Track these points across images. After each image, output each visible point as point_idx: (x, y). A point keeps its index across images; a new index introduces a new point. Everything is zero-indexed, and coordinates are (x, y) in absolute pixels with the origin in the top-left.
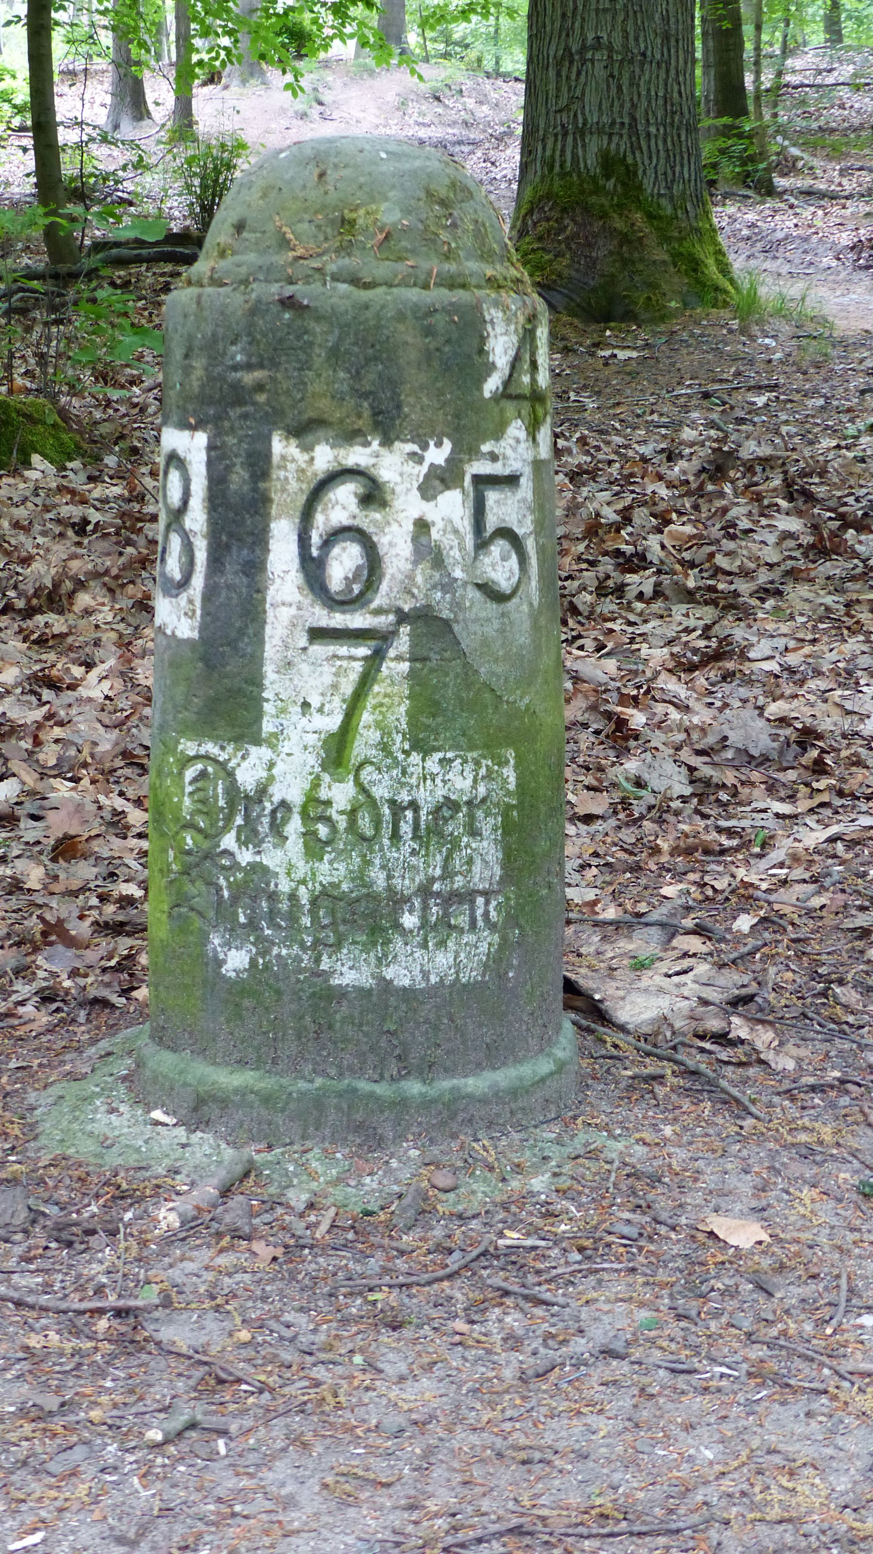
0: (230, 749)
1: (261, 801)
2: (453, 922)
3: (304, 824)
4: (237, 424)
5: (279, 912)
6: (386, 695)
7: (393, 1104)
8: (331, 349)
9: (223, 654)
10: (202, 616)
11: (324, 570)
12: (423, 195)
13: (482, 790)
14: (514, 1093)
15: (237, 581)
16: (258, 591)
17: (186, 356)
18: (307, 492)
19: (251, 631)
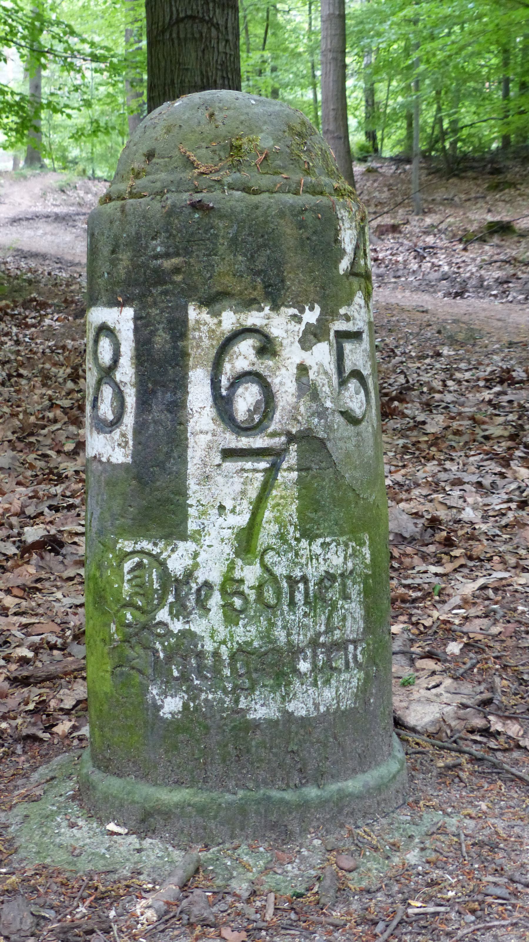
0: (161, 545)
1: (188, 583)
2: (334, 665)
3: (223, 598)
4: (158, 299)
5: (205, 666)
6: (282, 497)
7: (299, 806)
8: (232, 239)
9: (153, 473)
10: (134, 446)
11: (232, 404)
12: (286, 129)
13: (350, 565)
14: (379, 789)
15: (163, 417)
16: (181, 424)
17: (113, 252)
18: (217, 347)
19: (175, 454)
